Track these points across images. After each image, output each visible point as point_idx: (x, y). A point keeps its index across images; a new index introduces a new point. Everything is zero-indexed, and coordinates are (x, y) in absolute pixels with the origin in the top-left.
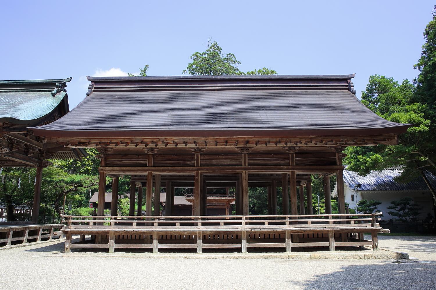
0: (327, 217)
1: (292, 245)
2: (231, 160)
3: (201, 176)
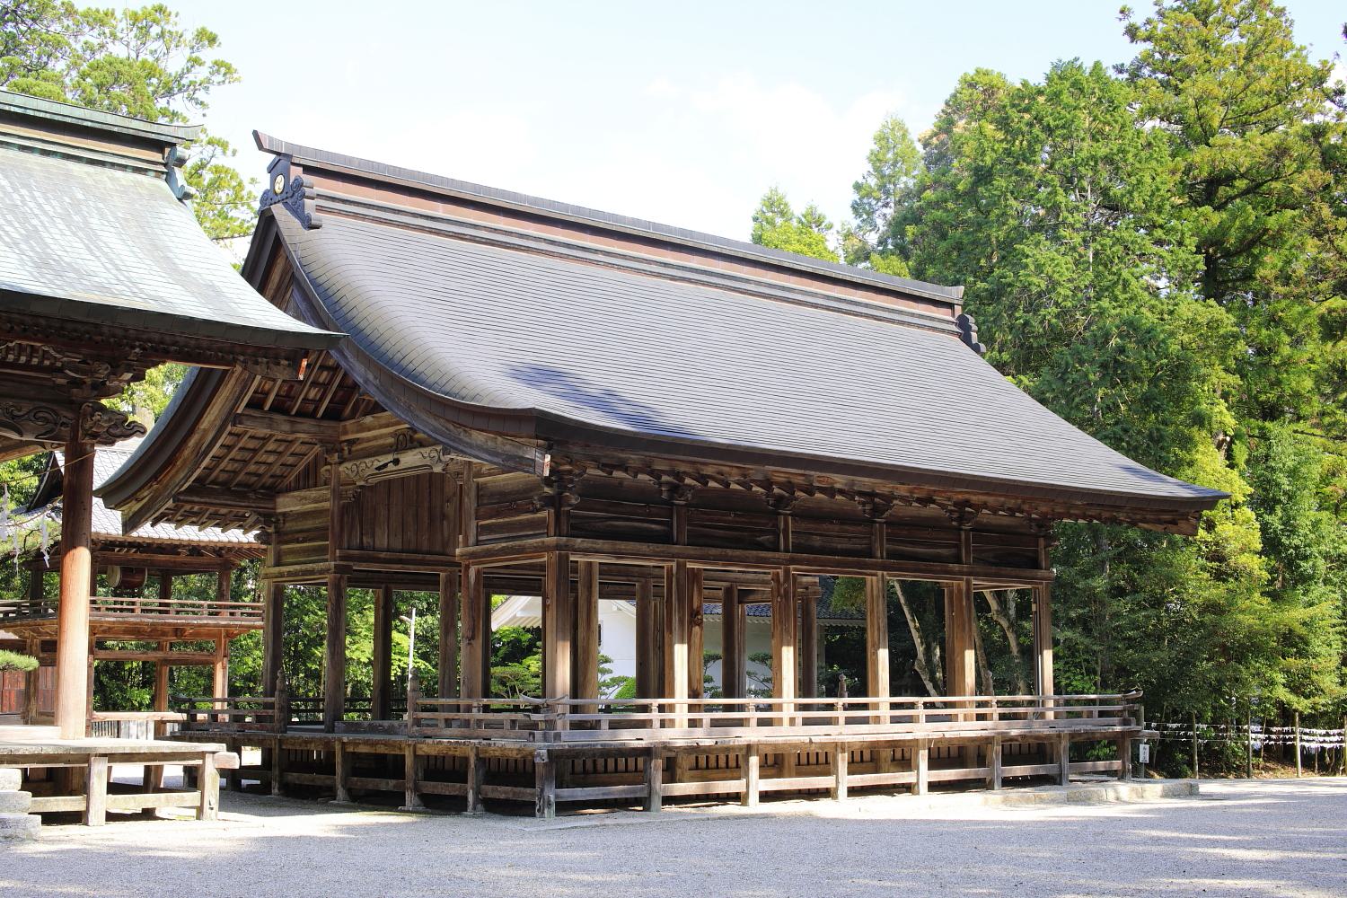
0: (831, 707)
1: (849, 781)
2: (850, 538)
3: (532, 567)
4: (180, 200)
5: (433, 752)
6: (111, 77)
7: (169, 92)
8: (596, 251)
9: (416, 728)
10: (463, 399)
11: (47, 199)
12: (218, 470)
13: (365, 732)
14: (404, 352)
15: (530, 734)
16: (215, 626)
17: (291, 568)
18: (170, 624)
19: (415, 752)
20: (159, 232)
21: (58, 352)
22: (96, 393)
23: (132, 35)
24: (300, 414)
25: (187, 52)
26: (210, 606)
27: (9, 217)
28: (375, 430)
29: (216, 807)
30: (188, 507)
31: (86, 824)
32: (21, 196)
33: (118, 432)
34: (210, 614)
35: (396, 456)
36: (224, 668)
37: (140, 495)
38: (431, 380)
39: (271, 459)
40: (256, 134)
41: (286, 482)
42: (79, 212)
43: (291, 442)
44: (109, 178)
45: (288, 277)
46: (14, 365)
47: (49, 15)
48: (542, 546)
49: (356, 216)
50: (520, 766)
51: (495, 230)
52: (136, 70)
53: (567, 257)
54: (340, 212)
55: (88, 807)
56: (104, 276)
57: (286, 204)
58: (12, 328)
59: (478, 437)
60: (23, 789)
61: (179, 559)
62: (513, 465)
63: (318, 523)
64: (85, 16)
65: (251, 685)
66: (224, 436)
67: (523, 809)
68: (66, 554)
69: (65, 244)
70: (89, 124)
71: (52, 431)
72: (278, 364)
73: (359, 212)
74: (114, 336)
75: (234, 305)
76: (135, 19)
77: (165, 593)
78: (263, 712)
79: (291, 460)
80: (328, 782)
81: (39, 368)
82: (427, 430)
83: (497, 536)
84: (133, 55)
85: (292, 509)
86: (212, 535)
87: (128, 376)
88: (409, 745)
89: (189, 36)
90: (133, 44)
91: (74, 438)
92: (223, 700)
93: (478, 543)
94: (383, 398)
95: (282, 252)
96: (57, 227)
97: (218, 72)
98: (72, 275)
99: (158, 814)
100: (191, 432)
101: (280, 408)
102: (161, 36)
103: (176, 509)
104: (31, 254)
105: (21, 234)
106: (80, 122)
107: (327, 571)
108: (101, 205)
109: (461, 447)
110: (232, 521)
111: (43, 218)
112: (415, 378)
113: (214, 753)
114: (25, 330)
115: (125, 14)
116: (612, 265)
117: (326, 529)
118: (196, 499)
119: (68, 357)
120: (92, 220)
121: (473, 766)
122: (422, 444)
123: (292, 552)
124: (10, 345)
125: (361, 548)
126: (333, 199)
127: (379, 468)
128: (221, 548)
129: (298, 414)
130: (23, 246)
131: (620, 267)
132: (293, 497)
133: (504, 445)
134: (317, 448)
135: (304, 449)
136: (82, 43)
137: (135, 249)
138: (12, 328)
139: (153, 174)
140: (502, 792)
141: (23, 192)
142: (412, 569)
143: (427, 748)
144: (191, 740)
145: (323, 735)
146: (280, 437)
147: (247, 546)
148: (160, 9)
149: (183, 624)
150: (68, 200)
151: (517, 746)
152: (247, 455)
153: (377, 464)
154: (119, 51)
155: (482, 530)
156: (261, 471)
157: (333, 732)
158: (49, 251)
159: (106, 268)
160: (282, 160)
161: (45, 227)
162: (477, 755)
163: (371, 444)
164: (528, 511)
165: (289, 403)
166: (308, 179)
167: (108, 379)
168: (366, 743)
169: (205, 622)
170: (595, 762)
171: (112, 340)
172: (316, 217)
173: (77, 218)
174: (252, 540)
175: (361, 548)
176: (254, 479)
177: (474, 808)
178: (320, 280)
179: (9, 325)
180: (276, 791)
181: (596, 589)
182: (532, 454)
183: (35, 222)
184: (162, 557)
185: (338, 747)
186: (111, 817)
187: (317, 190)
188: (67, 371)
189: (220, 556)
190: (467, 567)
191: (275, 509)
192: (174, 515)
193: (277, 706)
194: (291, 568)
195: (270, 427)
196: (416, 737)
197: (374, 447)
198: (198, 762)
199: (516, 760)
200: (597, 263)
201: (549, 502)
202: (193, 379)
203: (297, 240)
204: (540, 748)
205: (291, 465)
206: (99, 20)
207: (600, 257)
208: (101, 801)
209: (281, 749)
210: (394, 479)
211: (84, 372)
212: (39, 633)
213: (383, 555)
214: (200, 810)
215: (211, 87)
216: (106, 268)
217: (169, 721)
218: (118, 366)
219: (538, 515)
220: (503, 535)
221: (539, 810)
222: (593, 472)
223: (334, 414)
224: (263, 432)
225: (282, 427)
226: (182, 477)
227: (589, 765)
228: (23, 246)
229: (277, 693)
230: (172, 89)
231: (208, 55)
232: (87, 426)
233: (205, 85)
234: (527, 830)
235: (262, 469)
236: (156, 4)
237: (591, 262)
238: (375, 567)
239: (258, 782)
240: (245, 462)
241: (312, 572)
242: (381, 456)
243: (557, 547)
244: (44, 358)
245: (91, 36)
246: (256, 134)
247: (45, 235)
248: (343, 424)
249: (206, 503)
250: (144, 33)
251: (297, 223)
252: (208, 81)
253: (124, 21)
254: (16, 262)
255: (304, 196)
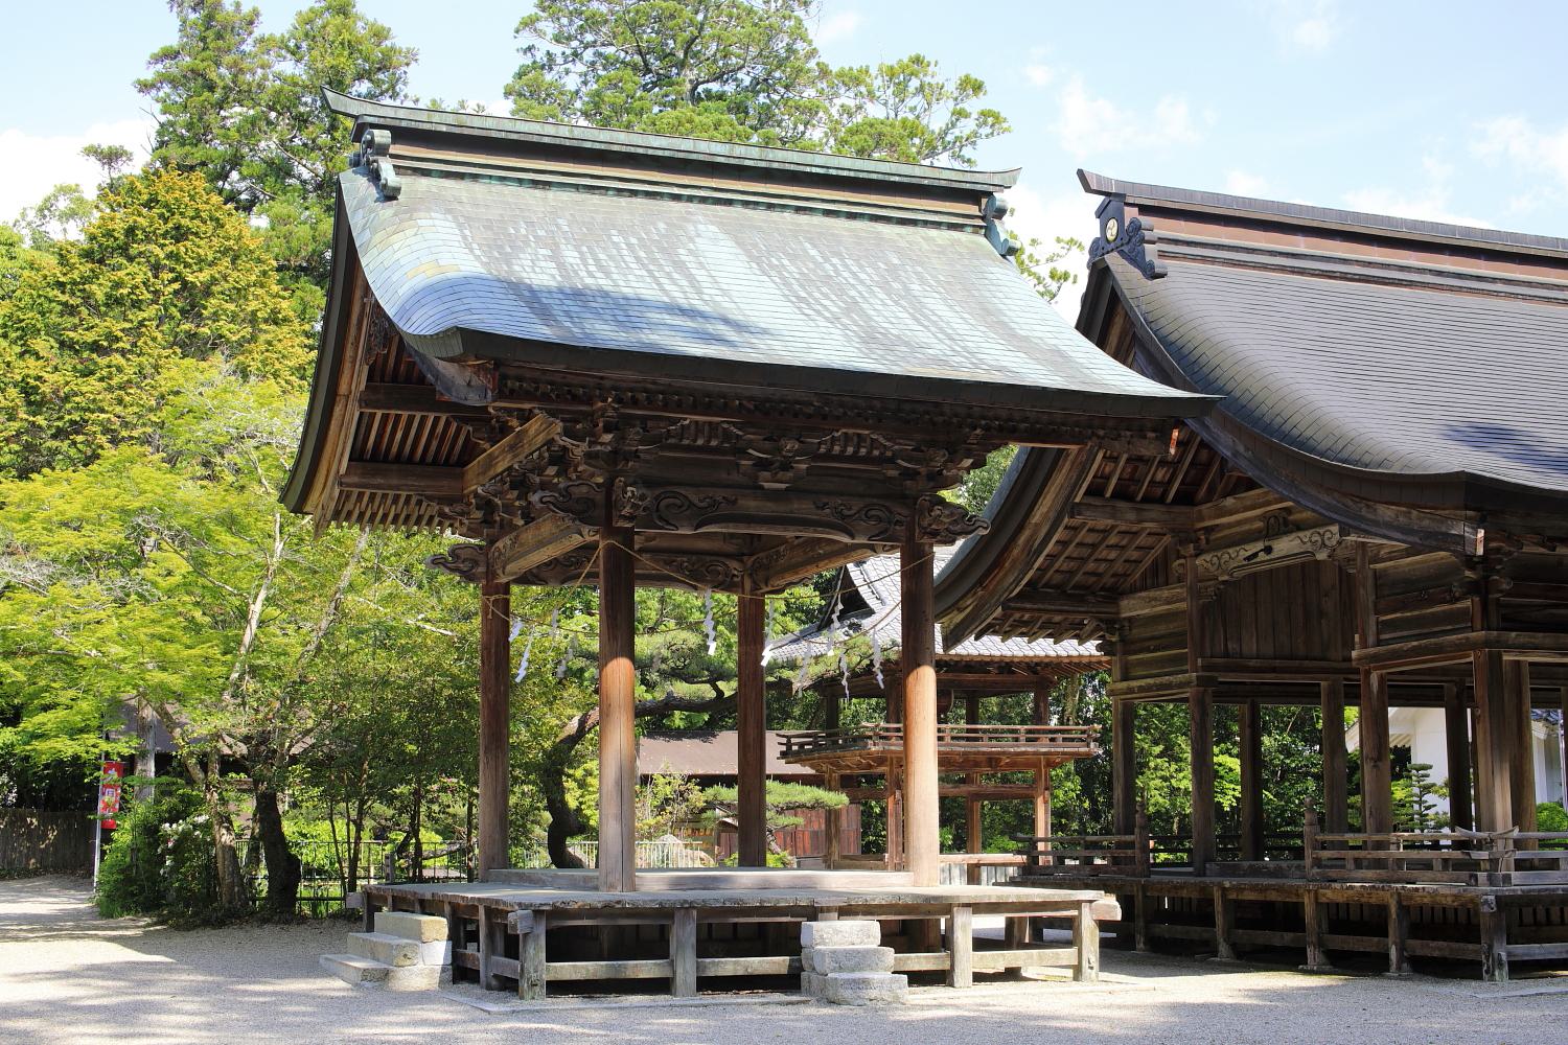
4: (1003, 256)
5: (1340, 899)
6: (877, 138)
7: (933, 153)
8: (1494, 280)
9: (1316, 870)
10: (1366, 466)
11: (861, 267)
12: (1051, 572)
13: (1244, 876)
14: (1285, 415)
15: (1471, 876)
16: (1035, 753)
17: (1142, 683)
18: (984, 753)
19: (1316, 898)
20: (988, 294)
21: (889, 440)
22: (932, 484)
23: (890, 92)
24: (1145, 500)
25: (951, 104)
26: (1029, 731)
27: (825, 290)
28: (1239, 513)
29: (1096, 965)
30: (1017, 616)
31: (952, 985)
32: (833, 265)
33: (958, 528)
34: (1028, 740)
35: (1267, 544)
36: (1046, 802)
37: (962, 604)
38: (1323, 447)
39: (1113, 555)
40: (1081, 174)
41: (1131, 580)
42: (897, 279)
43: (1135, 533)
44: (923, 238)
45: (1128, 339)
46: (841, 458)
47: (802, 80)
48: (1466, 645)
49: (1204, 259)
50: (1462, 918)
51: (1370, 264)
52: (898, 130)
53: (1460, 289)
54: (1185, 257)
55: (952, 966)
56: (938, 348)
57: (1121, 253)
58: (845, 413)
59: (1386, 512)
60: (883, 944)
61: (989, 678)
62: (1434, 543)
63: (1171, 627)
64: (841, 75)
65: (1063, 821)
66: (1061, 529)
67: (1467, 970)
68: (909, 674)
69: (890, 317)
70: (897, 179)
71: (886, 530)
72: (1145, 437)
73: (1207, 254)
74: (956, 415)
75: (1088, 371)
76: (891, 73)
77: (972, 718)
78: (1121, 853)
79: (1135, 555)
80: (1206, 936)
81: (868, 460)
82: (1317, 508)
83: (1405, 633)
84: (892, 115)
85: (1139, 612)
86: (1044, 648)
87: (968, 462)
88: (1309, 891)
89: (951, 87)
90: (891, 102)
91: (911, 538)
92: (1045, 840)
93: (1379, 643)
94: (1257, 473)
95: (1120, 309)
96: (876, 297)
97: (985, 123)
98: (904, 349)
99: (1024, 974)
100: (1020, 528)
101: (1122, 494)
102: (921, 90)
103: (1004, 618)
104: (855, 328)
105: (839, 307)
106: (887, 178)
107: (1188, 684)
108: (920, 269)
109: (1363, 526)
110: (1067, 630)
111: (860, 288)
112: (1302, 445)
113: (1091, 902)
114: (859, 415)
115: (880, 69)
116: (1515, 296)
117: (1183, 634)
118: (1028, 606)
119: (900, 444)
120: (912, 286)
121: (1394, 916)
122: (1299, 527)
123: (1141, 663)
124: (836, 435)
125: (1227, 655)
126: (1176, 242)
127: (1248, 558)
128: (1037, 664)
129: (1145, 500)
130: (845, 320)
131: (1525, 297)
132: (1143, 598)
133: (1420, 520)
134: (1167, 539)
135: (1151, 540)
136: (837, 107)
137: (966, 316)
138: (845, 413)
139: (969, 229)
140: (1435, 948)
141: (835, 260)
142: (1287, 679)
143: (1334, 893)
144: (1034, 885)
145: (1192, 880)
146: (1123, 528)
147: (1067, 661)
148: (917, 60)
149: (999, 753)
150: (882, 266)
151: (1455, 891)
152: (1085, 552)
153: (1244, 554)
154: (875, 111)
155: (1384, 626)
156: (1101, 570)
157: (1205, 875)
158: (873, 323)
159: (937, 338)
160: (1113, 201)
161: (864, 297)
162: (1399, 902)
163: (1234, 530)
164: (1444, 601)
165: (1133, 487)
166: (1146, 220)
167: (946, 468)
168: (1254, 888)
169: (1023, 749)
170: (1548, 911)
171: (955, 420)
172: (1160, 264)
173: (896, 285)
174: (1095, 653)
175: (1227, 655)
176: (1093, 579)
177: (1399, 968)
178: (1172, 338)
179: (841, 410)
180: (1142, 945)
181: (1528, 696)
182: (1459, 529)
183: (853, 293)
184: (970, 677)
185: (1217, 895)
186: (979, 978)
187: (1158, 233)
188: (899, 461)
189: (1035, 673)
190: (1368, 673)
191: (1118, 613)
192: (1001, 626)
193: (1137, 845)
194: (1142, 683)
195: (1113, 517)
196: (1317, 880)
197: (1237, 533)
198: (1074, 913)
199: (1456, 909)
200: (1496, 294)
201: (1473, 588)
202: (1021, 465)
203: (1139, 293)
204: (1485, 891)
205: (1135, 561)
206: (852, 79)
207: (1499, 287)
208: (968, 960)
209: (1145, 897)
210: (1277, 569)
211: (918, 461)
212: (839, 767)
213: (1252, 663)
214: (1078, 971)
215: (979, 141)
216: (937, 338)
217: (984, 865)
218: (956, 452)
219: (1458, 605)
220: (1399, 634)
221: (1487, 972)
222: (1532, 549)
223: (1186, 498)
224: (1104, 522)
225: (1128, 516)
226: (1013, 581)
227: (1541, 916)
228: (845, 320)
229: (1136, 830)
230: (935, 148)
231: (974, 105)
232: (925, 523)
233: (971, 140)
234: (1480, 996)
235: (1102, 567)
236: (913, 54)
237: (1489, 293)
238: (1246, 678)
239: (1114, 935)
240: (1083, 560)
241: (1169, 686)
242: (1249, 544)
243: (1487, 643)
244: (872, 448)
245: (847, 99)
246: (1081, 174)
247: (865, 306)
248: (1196, 509)
249: (1039, 610)
250: (901, 91)
251: (1137, 273)
252: (975, 134)
253: (880, 78)
254: (841, 338)
255: (1143, 241)
